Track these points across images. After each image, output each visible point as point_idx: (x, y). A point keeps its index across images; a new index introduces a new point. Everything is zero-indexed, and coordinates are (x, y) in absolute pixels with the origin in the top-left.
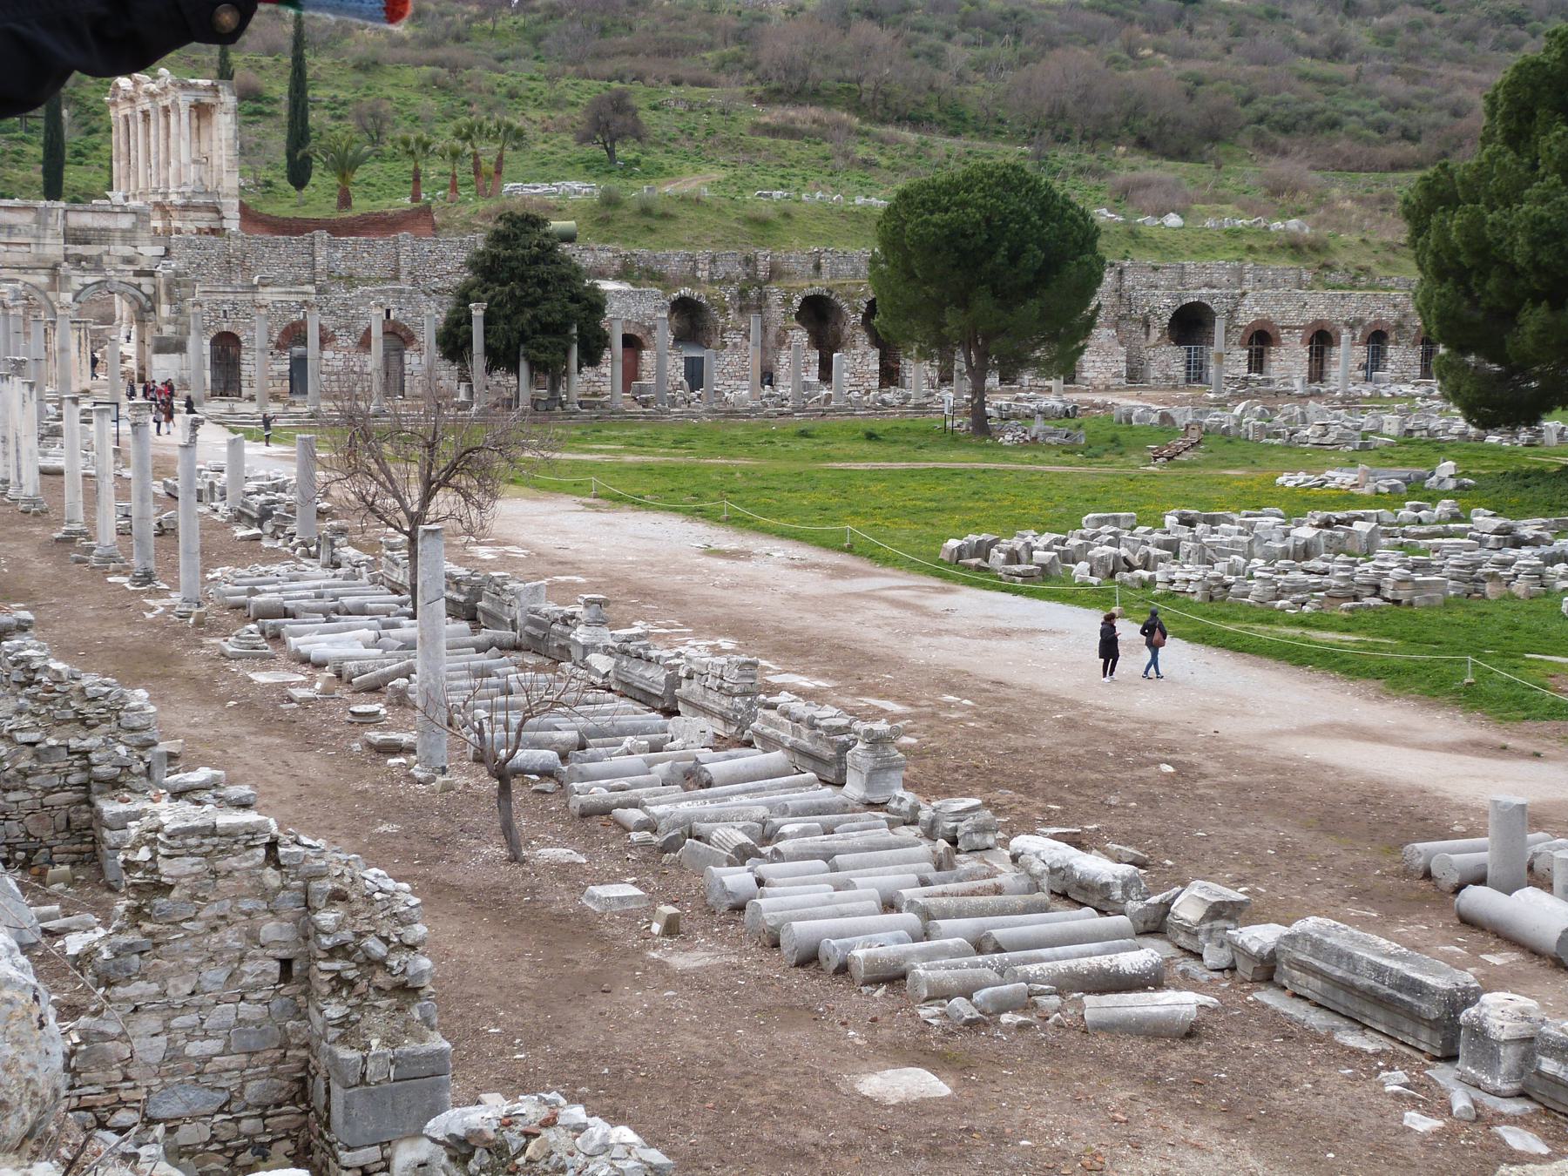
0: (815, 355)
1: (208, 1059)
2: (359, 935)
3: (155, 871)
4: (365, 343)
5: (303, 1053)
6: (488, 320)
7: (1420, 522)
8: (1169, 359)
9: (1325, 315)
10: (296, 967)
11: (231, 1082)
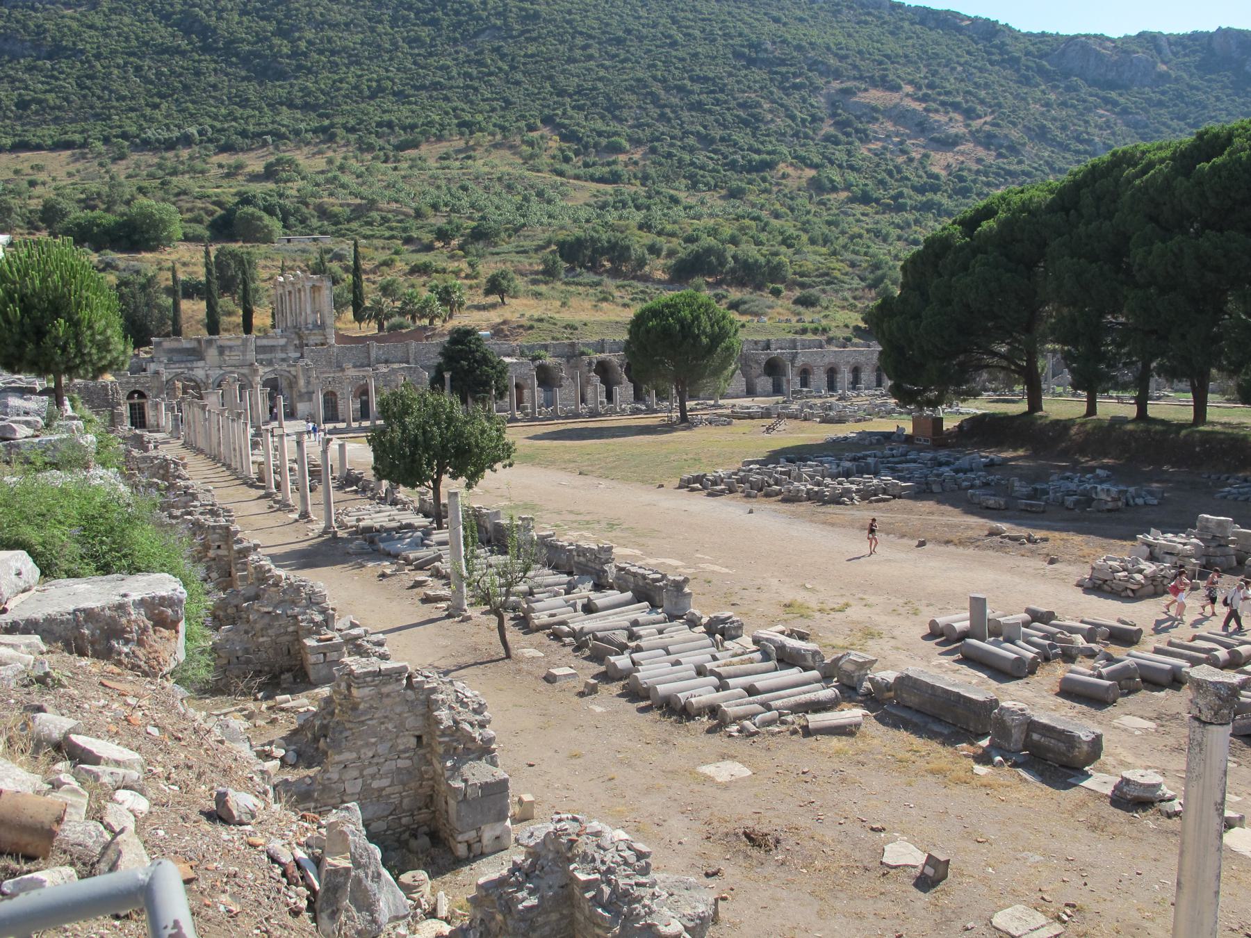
1: (383, 789)
5: (431, 782)
7: (893, 456)
8: (765, 382)
9: (833, 360)
10: (425, 740)
11: (395, 799)
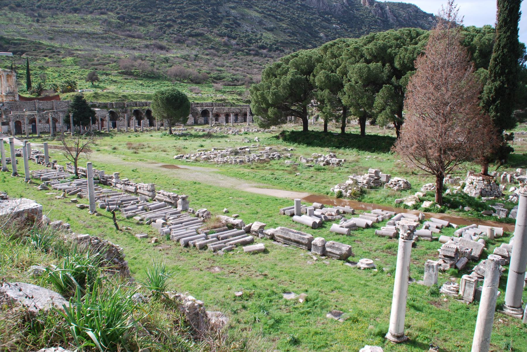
0: (137, 121)
4: (48, 122)
6: (73, 116)
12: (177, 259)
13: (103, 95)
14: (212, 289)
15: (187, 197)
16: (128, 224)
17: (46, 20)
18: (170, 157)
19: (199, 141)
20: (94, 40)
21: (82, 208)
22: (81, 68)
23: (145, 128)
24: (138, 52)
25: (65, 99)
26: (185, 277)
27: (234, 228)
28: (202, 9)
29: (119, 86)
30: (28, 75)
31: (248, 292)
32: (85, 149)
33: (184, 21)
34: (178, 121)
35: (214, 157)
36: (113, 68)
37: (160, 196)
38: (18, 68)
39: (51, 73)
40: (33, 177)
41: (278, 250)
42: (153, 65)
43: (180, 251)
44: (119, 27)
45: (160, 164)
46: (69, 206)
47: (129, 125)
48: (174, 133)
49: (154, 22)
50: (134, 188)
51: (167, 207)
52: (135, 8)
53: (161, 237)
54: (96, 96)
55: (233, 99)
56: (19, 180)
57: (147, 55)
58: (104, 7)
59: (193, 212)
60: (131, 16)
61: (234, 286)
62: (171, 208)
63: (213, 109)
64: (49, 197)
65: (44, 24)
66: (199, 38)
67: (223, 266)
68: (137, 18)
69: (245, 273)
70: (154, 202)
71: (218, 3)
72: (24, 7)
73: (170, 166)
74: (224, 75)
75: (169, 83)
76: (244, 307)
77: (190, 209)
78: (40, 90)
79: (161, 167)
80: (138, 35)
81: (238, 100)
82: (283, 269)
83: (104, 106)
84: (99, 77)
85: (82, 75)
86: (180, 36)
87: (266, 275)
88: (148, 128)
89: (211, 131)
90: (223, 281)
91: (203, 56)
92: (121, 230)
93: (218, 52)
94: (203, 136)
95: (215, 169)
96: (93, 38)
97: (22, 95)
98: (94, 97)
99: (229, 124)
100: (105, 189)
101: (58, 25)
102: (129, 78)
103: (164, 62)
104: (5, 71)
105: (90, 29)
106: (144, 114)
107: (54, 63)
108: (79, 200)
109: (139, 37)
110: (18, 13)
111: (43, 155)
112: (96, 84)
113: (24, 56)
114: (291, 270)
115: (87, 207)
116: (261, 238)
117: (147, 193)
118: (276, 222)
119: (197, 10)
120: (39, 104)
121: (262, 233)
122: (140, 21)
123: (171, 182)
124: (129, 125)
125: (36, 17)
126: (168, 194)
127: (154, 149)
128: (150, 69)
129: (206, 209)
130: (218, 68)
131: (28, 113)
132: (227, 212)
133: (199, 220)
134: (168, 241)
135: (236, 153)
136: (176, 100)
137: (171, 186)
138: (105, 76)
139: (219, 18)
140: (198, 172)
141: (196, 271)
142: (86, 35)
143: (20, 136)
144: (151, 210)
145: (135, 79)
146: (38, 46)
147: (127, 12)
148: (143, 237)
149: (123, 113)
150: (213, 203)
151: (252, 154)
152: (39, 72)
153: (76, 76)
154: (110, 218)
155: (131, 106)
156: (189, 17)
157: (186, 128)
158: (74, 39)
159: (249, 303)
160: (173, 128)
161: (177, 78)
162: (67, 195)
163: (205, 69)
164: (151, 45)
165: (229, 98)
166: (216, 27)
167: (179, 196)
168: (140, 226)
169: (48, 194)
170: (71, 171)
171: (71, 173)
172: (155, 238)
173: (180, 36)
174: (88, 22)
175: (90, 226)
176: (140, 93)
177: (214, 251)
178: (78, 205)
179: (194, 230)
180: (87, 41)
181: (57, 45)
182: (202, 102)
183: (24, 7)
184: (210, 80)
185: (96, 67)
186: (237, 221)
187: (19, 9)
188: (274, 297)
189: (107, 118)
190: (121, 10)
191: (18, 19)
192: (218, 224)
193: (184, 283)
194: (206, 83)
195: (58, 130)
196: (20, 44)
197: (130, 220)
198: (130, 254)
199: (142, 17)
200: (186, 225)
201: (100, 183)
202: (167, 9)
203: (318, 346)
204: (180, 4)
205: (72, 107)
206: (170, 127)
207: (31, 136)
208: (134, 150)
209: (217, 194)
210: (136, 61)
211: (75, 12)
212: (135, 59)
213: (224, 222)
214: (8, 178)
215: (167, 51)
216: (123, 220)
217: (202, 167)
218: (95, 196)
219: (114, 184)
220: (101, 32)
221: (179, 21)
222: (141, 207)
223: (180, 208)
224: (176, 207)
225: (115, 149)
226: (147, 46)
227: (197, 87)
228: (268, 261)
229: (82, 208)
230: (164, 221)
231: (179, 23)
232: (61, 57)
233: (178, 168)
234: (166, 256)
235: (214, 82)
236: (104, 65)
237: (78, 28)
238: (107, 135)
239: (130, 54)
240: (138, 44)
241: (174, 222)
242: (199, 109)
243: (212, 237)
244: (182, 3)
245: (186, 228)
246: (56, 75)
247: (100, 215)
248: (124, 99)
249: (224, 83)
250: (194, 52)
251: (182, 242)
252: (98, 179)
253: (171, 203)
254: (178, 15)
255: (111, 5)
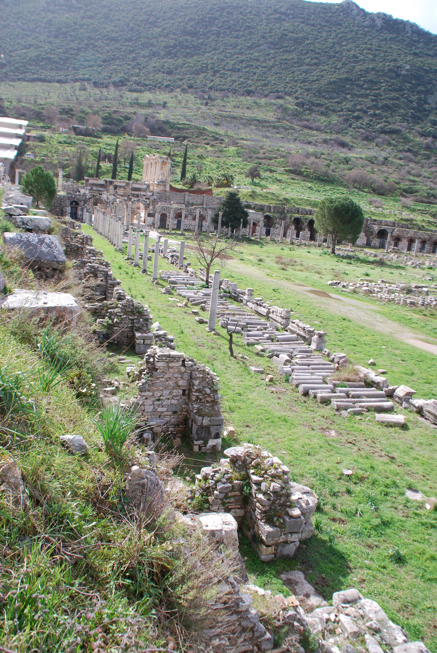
0: (295, 232)
1: (163, 412)
2: (204, 387)
3: (154, 364)
4: (194, 219)
6: (223, 216)
12: (288, 407)
13: (261, 195)
14: (317, 457)
15: (325, 334)
16: (246, 352)
17: (215, 103)
18: (324, 282)
19: (365, 268)
20: (264, 129)
21: (201, 322)
22: (243, 161)
23: (303, 242)
24: (314, 147)
25: (218, 195)
26: (290, 432)
27: (372, 387)
28: (405, 98)
29: (282, 187)
30: (185, 163)
31: (360, 473)
32: (221, 255)
33: (377, 112)
34: (345, 239)
35: (378, 292)
36: (280, 164)
37: (293, 327)
38: (175, 155)
39: (209, 163)
40: (161, 278)
41: (421, 430)
42: (328, 165)
43: (296, 399)
44: (296, 115)
45: (309, 289)
46: (187, 317)
47: (285, 235)
48: (337, 252)
49: (339, 111)
50: (266, 310)
51: (299, 342)
52: (319, 93)
53: (279, 377)
54: (253, 195)
55: (423, 221)
56: (148, 278)
57: (324, 152)
58: (282, 89)
59: (328, 355)
60: (312, 103)
61: (347, 460)
62: (302, 344)
63: (393, 230)
64: (169, 303)
65: (212, 107)
66: (394, 136)
67: (342, 431)
68: (319, 105)
69: (366, 448)
70: (286, 333)
71: (428, 91)
72: (196, 88)
73: (321, 292)
74: (417, 187)
75: (345, 190)
76: (349, 492)
77: (326, 350)
78: (194, 181)
79: (309, 291)
80: (316, 126)
81: (429, 222)
82: (420, 458)
83: (261, 209)
84: (261, 173)
85: (242, 169)
86: (370, 132)
87: (393, 458)
88: (307, 242)
89: (385, 257)
90: (335, 450)
91: (395, 160)
92: (235, 357)
93: (416, 157)
94: (373, 263)
95: (375, 307)
96: (264, 126)
97: (174, 185)
98: (251, 196)
99: (411, 252)
100: (233, 306)
101: (226, 110)
102: (296, 178)
103: (343, 162)
104: (161, 158)
105: (261, 116)
106: (306, 224)
107: (215, 152)
108: (201, 312)
109: (318, 129)
110: (189, 95)
111: (179, 254)
112: (256, 180)
113: (185, 142)
114: (431, 461)
115: (206, 323)
116: (405, 408)
117: (279, 319)
118: (433, 392)
119: (398, 99)
120: (189, 198)
121: (408, 402)
122: (323, 109)
123: (315, 312)
124: (285, 235)
125: (205, 99)
126: (304, 325)
127: (307, 269)
128: (324, 169)
129: (343, 355)
130: (412, 178)
131: (175, 206)
132: (373, 364)
133: (332, 366)
134: (286, 384)
135: (409, 291)
136: (347, 212)
137: (313, 317)
138: (268, 172)
139: (426, 111)
140: (353, 306)
141: (306, 428)
142: (256, 122)
143: (163, 230)
144: (278, 341)
145: (304, 180)
146: (201, 132)
147: (308, 97)
148: (258, 371)
149: (281, 219)
150: (358, 349)
151: (430, 297)
152: (196, 162)
153: (236, 169)
154: (226, 339)
155: (292, 212)
156: (386, 108)
157: (354, 248)
158: (241, 126)
159: (357, 489)
160: (337, 247)
161: (356, 185)
162: (189, 304)
163: (394, 177)
164: (331, 140)
165: (418, 218)
166: (418, 123)
167: (316, 331)
168: (259, 358)
169: (170, 299)
170: (202, 277)
171: (203, 280)
172: (270, 376)
173: (370, 132)
174: (260, 107)
175: (202, 345)
176: (306, 198)
177: (337, 410)
178: (197, 318)
179: (321, 377)
180: (256, 129)
181: (222, 132)
182: (381, 219)
183: (196, 88)
184: (398, 192)
185: (260, 161)
186: (380, 379)
187: (191, 90)
188: (393, 490)
189: (261, 224)
190: (301, 94)
191: (187, 101)
192: (353, 377)
193: (286, 439)
194: (392, 196)
195: (204, 229)
196: (184, 129)
197: (250, 348)
198: (236, 388)
199: (326, 104)
200: (313, 369)
201: (230, 297)
202: (358, 96)
203: (428, 576)
204: (376, 90)
205: (224, 205)
206: (334, 245)
207: (174, 232)
208: (283, 266)
209: (367, 338)
210: (308, 158)
211: (248, 95)
212: (308, 155)
213: (362, 375)
214: (137, 275)
215: (350, 150)
216: (241, 346)
217: (359, 301)
218: (217, 311)
219: (244, 302)
220: (273, 119)
221: (371, 112)
222: (267, 335)
223: (313, 346)
224: (310, 345)
225: (260, 260)
226: (325, 141)
227: (379, 199)
228: (404, 440)
229: (201, 322)
230: (288, 358)
231: (371, 115)
232: (223, 145)
233: (330, 297)
234: (277, 401)
235: (403, 196)
236: (270, 159)
237: (248, 114)
238: (257, 243)
239: (303, 149)
240: (315, 138)
241: (300, 362)
242: (376, 228)
243: (341, 392)
244: (380, 89)
245: (312, 373)
246: (214, 166)
247: (218, 334)
248: (285, 202)
249: (415, 198)
250: (385, 154)
251: (301, 388)
252: (229, 293)
253: (304, 338)
254: (371, 104)
255: (291, 87)
